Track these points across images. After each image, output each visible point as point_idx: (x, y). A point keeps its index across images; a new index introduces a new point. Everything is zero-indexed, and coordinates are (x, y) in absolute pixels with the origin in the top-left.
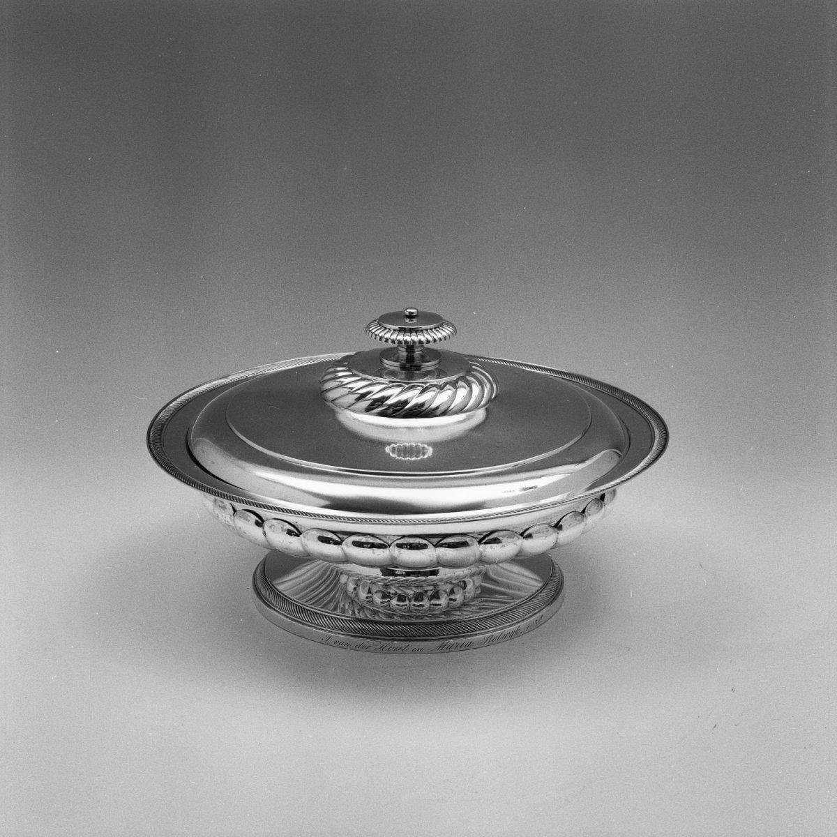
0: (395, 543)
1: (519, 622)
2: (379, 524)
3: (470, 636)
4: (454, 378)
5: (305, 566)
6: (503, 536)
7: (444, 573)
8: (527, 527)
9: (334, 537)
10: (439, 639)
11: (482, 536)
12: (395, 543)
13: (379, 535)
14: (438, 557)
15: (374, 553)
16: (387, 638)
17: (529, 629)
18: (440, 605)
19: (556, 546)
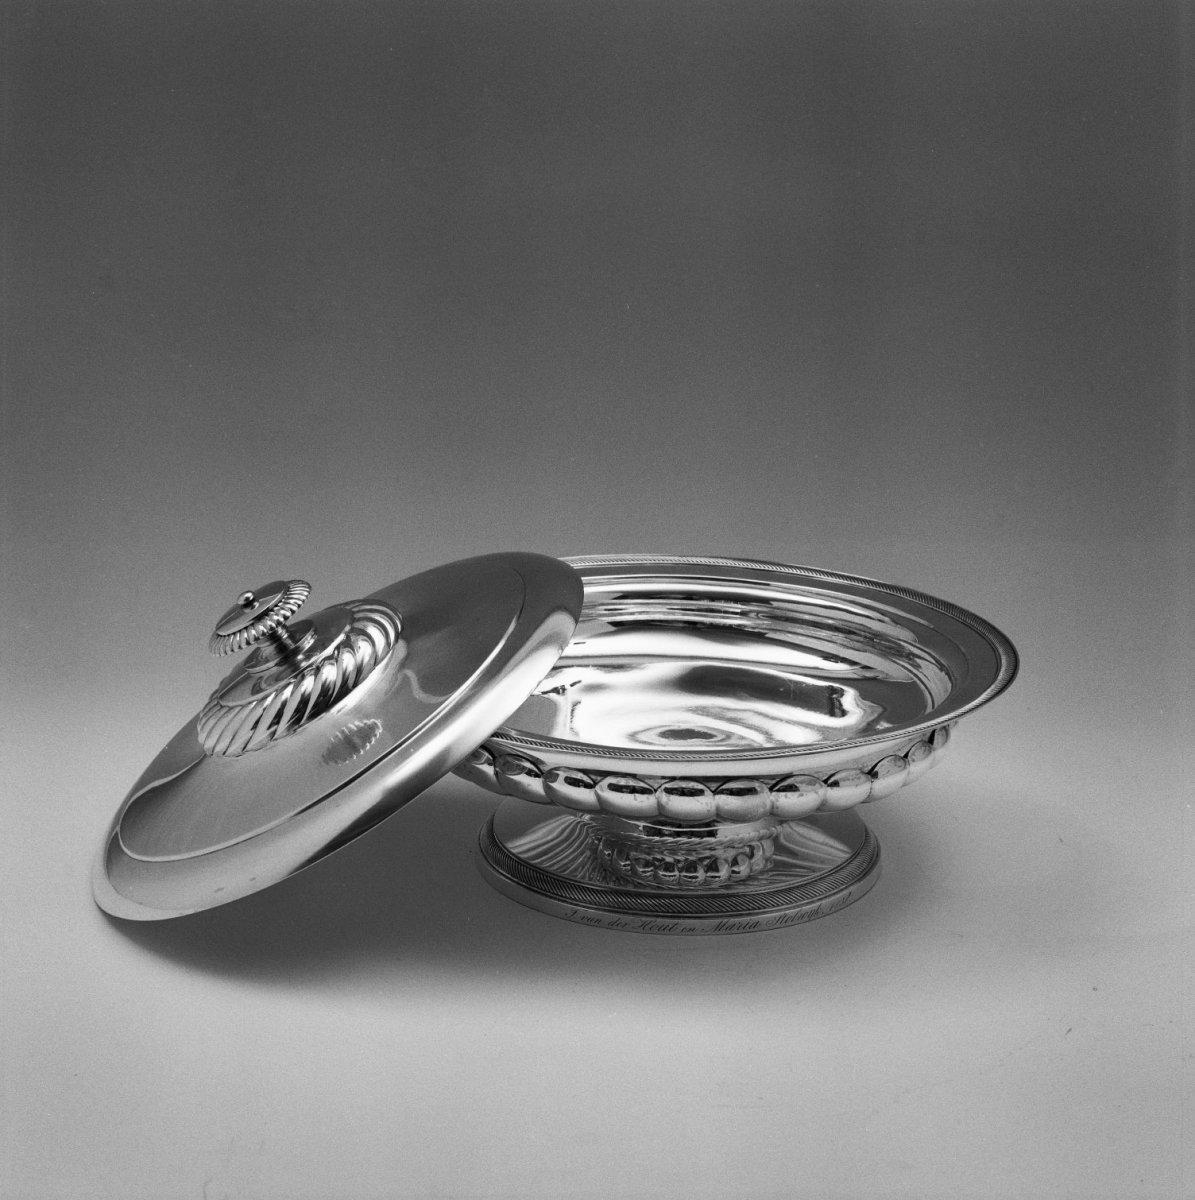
0: (663, 787)
1: (821, 899)
2: (643, 760)
3: (757, 914)
4: (341, 637)
5: (541, 828)
6: (801, 783)
7: (726, 832)
8: (832, 772)
9: (586, 778)
10: (718, 917)
11: (774, 782)
12: (663, 787)
13: (640, 775)
14: (718, 808)
15: (635, 799)
16: (649, 913)
17: (835, 909)
18: (719, 877)
19: (869, 799)
